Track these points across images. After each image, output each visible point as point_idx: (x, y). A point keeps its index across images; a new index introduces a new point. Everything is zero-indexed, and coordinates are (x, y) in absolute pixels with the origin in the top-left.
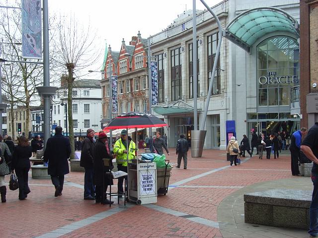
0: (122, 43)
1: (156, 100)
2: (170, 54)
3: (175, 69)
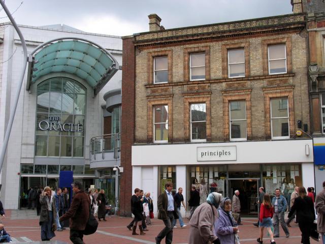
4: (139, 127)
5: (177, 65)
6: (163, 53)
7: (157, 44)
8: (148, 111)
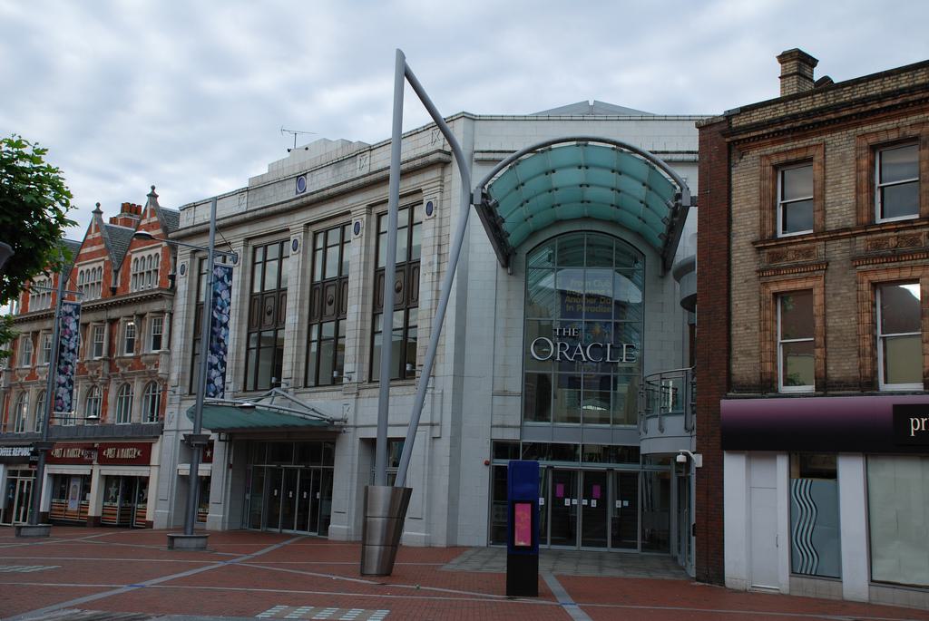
0: (92, 215)
4: (741, 352)
5: (839, 182)
6: (800, 155)
7: (784, 131)
8: (760, 310)
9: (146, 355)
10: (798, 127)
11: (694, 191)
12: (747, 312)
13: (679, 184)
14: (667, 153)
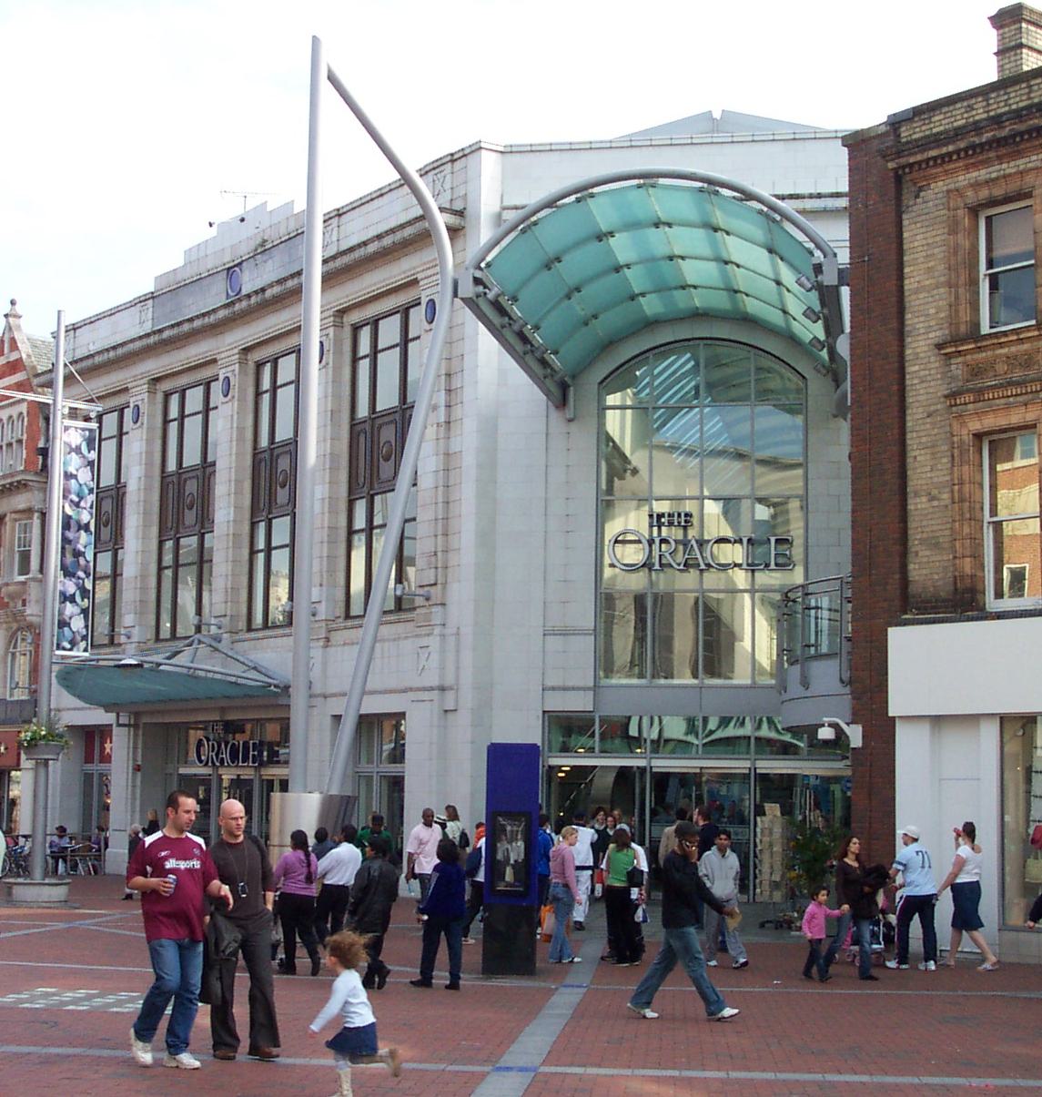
1: (78, 624)
2: (159, 407)
3: (273, 460)
4: (922, 541)
6: (1013, 187)
7: (982, 145)
9: (7, 584)
10: (1005, 138)
11: (844, 257)
12: (932, 470)
13: (818, 246)
14: (819, 196)
